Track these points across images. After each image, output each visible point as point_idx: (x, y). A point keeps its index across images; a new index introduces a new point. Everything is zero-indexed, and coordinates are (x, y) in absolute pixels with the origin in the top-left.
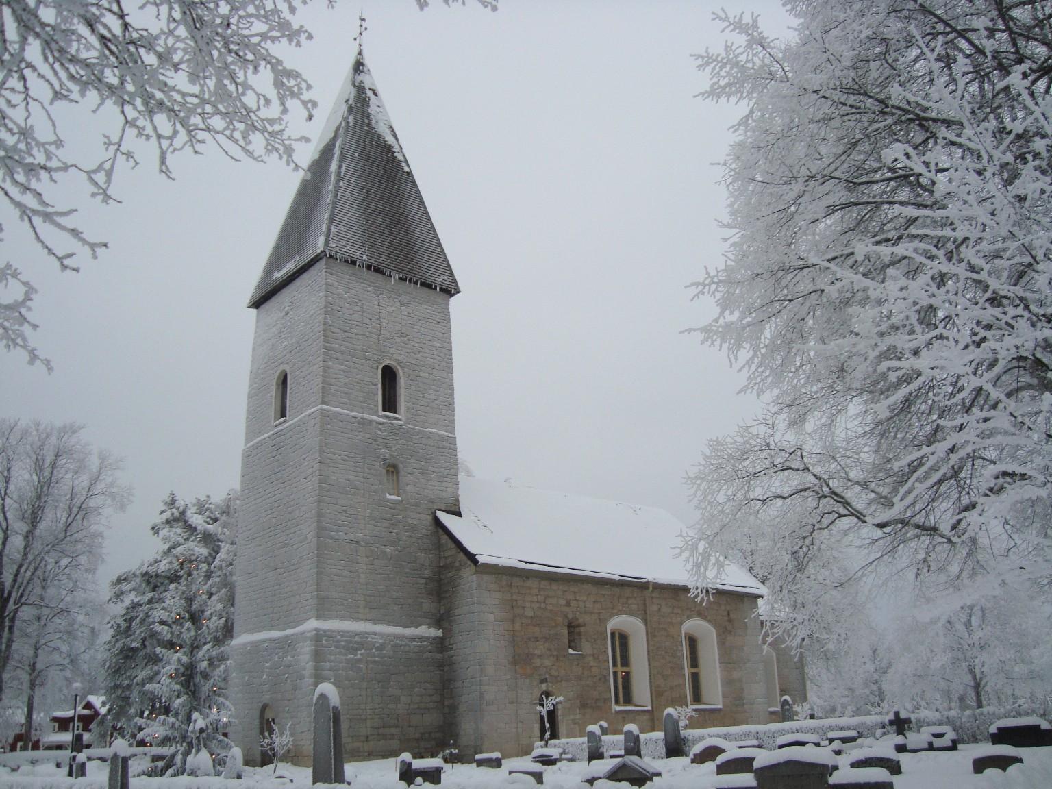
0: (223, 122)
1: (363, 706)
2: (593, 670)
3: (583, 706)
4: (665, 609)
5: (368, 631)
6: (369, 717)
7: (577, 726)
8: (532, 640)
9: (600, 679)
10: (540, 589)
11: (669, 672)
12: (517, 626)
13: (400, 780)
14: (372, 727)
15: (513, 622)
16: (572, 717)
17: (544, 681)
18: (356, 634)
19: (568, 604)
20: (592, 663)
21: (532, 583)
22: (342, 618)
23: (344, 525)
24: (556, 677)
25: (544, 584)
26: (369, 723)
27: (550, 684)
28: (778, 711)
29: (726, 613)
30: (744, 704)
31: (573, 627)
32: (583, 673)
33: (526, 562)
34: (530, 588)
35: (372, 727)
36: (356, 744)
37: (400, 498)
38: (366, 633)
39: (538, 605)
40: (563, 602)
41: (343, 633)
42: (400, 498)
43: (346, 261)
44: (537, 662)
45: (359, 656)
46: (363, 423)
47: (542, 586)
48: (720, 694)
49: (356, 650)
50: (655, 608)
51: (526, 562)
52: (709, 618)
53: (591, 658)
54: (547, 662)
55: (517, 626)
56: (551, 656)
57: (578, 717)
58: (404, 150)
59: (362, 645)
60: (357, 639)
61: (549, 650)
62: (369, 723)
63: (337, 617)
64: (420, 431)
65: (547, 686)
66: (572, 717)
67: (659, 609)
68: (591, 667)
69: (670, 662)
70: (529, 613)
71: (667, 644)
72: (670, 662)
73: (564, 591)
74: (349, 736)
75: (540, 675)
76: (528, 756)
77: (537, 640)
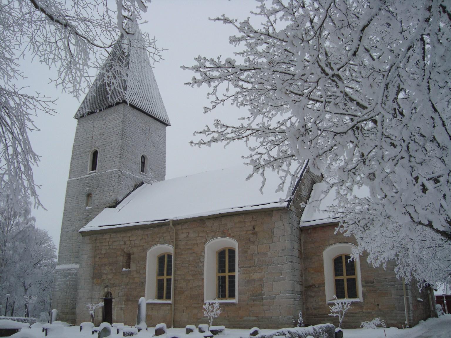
0: (239, 64)
1: (67, 300)
2: (136, 279)
3: (127, 300)
4: (192, 235)
5: (72, 268)
6: (68, 304)
7: (123, 311)
8: (103, 265)
9: (139, 285)
10: (110, 238)
11: (191, 278)
12: (97, 259)
13: (258, 334)
14: (69, 309)
15: (95, 257)
16: (120, 306)
17: (107, 286)
18: (68, 269)
19: (125, 244)
20: (135, 276)
21: (107, 236)
22: (65, 264)
23: (69, 225)
24: (114, 284)
25: (113, 235)
26: (68, 307)
27: (109, 288)
28: (360, 302)
29: (251, 228)
30: (262, 299)
31: (129, 256)
32: (129, 281)
33: (101, 226)
34: (105, 239)
35: (69, 309)
36: (63, 316)
37: (91, 207)
38: (71, 269)
39: (108, 247)
40: (122, 243)
41: (64, 270)
42: (91, 207)
43: (81, 117)
44: (104, 277)
45: (68, 279)
46: (81, 180)
47: (112, 236)
48: (326, 286)
49: (67, 276)
50: (184, 235)
51: (101, 226)
52: (232, 234)
53: (135, 273)
54: (109, 277)
55: (97, 259)
56: (112, 273)
57: (123, 306)
58: (152, 48)
59: (69, 274)
60: (68, 272)
61: (112, 270)
62: (68, 307)
63: (63, 264)
64: (103, 173)
65: (108, 289)
66: (120, 306)
67: (187, 236)
68: (134, 278)
69: (191, 271)
70: (104, 252)
71: (191, 259)
72: (191, 271)
73: (123, 237)
74: (61, 312)
75: (105, 283)
76: (154, 328)
77: (105, 265)
